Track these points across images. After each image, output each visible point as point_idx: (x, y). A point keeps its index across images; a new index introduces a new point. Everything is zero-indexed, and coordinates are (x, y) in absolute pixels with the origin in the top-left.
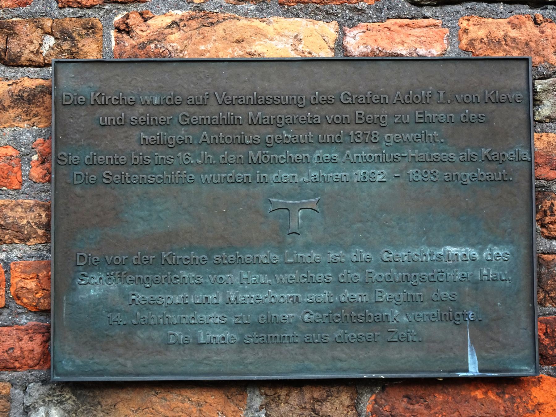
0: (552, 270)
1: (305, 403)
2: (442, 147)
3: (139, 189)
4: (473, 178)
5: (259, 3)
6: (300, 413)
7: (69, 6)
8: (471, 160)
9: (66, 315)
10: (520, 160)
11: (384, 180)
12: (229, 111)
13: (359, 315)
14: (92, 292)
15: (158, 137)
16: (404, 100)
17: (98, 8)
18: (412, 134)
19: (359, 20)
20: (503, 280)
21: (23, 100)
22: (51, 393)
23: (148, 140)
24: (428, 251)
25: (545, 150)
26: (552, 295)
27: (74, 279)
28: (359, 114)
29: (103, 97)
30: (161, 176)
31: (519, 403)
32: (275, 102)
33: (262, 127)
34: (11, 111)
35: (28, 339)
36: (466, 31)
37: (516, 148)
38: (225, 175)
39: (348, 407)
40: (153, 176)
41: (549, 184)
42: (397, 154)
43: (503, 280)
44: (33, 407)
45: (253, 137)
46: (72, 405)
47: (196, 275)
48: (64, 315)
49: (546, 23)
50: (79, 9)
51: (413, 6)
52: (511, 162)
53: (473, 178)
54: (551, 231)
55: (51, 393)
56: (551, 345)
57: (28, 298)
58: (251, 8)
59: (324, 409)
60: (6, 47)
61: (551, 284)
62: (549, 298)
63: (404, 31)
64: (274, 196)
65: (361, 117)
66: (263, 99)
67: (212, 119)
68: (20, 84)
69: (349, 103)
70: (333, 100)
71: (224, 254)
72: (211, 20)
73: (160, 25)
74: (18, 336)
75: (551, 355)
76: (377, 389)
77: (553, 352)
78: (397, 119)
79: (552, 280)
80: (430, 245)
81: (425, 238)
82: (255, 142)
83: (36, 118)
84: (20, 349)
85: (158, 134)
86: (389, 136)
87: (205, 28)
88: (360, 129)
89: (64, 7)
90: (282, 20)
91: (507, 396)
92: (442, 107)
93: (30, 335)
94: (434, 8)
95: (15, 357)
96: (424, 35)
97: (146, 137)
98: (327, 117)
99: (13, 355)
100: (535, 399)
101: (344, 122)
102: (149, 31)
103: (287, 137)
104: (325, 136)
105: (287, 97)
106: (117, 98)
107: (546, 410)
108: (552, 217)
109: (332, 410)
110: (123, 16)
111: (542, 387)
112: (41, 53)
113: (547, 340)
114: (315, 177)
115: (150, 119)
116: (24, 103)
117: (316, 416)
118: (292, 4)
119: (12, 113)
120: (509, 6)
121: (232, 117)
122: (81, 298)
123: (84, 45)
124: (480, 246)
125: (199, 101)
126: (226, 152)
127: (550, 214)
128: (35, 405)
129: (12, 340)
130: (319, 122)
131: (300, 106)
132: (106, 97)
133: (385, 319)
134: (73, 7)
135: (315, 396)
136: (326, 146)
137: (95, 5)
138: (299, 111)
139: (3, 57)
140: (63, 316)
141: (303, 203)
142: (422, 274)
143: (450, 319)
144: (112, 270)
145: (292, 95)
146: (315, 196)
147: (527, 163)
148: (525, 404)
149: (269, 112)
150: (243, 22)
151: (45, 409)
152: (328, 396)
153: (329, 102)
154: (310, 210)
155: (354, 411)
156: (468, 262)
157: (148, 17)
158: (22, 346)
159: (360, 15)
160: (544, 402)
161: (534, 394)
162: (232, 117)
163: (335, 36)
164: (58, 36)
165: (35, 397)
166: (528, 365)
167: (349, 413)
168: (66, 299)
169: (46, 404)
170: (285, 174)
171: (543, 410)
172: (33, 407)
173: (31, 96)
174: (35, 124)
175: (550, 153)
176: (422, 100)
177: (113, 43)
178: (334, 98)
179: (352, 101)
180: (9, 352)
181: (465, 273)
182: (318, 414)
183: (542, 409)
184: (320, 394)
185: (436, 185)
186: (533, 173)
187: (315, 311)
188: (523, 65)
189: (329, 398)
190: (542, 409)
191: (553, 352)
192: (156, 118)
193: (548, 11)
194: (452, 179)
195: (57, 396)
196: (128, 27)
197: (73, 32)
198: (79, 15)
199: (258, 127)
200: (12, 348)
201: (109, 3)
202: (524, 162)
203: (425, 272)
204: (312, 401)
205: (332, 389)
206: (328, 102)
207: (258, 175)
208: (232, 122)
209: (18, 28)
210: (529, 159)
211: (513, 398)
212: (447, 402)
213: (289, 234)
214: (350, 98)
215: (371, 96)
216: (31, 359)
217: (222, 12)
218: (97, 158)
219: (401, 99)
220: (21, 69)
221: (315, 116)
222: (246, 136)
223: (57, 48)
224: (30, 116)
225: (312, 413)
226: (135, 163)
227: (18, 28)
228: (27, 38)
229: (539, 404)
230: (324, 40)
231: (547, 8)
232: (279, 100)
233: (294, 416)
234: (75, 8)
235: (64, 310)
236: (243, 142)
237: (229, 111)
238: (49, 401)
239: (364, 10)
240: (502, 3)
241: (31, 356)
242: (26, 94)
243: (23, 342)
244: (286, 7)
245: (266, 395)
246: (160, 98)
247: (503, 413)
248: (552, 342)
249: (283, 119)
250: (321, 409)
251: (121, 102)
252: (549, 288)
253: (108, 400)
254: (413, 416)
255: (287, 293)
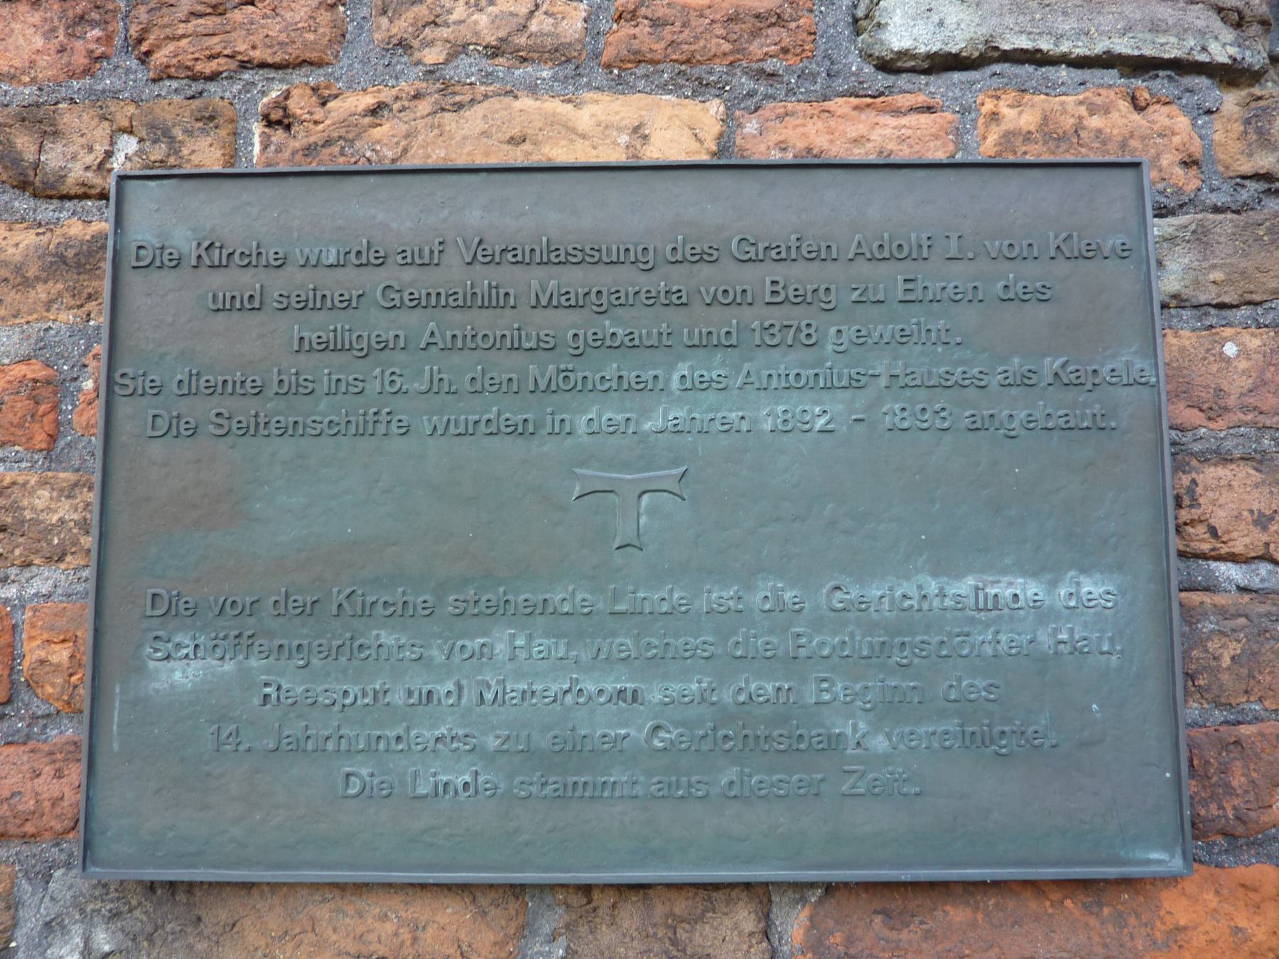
0: (1199, 626)
1: (655, 925)
2: (958, 354)
3: (286, 448)
4: (1029, 422)
5: (559, 65)
6: (643, 948)
7: (170, 77)
8: (1026, 381)
9: (119, 726)
10: (1131, 381)
11: (830, 427)
12: (485, 278)
13: (776, 733)
14: (178, 675)
15: (331, 335)
16: (872, 253)
17: (226, 78)
18: (891, 326)
19: (767, 97)
20: (1102, 653)
21: (65, 263)
22: (97, 893)
23: (310, 342)
24: (932, 587)
25: (1174, 365)
26: (1201, 682)
27: (140, 646)
28: (772, 282)
29: (217, 251)
30: (336, 419)
31: (1135, 927)
32: (589, 256)
33: (561, 312)
34: (40, 287)
35: (53, 773)
36: (994, 117)
37: (1123, 355)
38: (476, 417)
39: (751, 934)
40: (318, 419)
41: (1184, 439)
42: (858, 370)
43: (1102, 653)
44: (58, 924)
45: (538, 334)
46: (141, 921)
47: (409, 639)
48: (115, 728)
49: (1157, 107)
50: (190, 82)
51: (880, 72)
52: (1111, 388)
53: (1029, 422)
54: (1191, 540)
55: (97, 893)
56: (1203, 795)
57: (53, 685)
58: (545, 74)
59: (698, 939)
60: (39, 159)
61: (1198, 659)
62: (1193, 689)
63: (863, 117)
64: (583, 464)
65: (778, 288)
66: (562, 252)
67: (448, 296)
68: (58, 231)
69: (750, 259)
70: (715, 253)
71: (472, 592)
72: (458, 98)
73: (353, 109)
74: (32, 768)
75: (1203, 817)
76: (813, 894)
77: (1207, 811)
78: (858, 292)
79: (1201, 649)
80: (935, 574)
81: (924, 557)
82: (542, 345)
83: (94, 303)
84: (33, 794)
85: (332, 328)
86: (839, 331)
87: (447, 115)
88: (777, 316)
89: (160, 79)
90: (605, 97)
91: (1106, 911)
92: (957, 267)
93: (57, 766)
94: (923, 77)
95: (24, 812)
96: (908, 124)
97: (306, 334)
98: (702, 289)
99: (20, 808)
100: (1168, 918)
101: (741, 300)
102: (328, 122)
103: (613, 334)
104: (697, 331)
105: (614, 248)
106: (247, 253)
107: (1195, 943)
108: (1193, 510)
109: (716, 942)
110: (279, 93)
111: (1183, 888)
112: (110, 170)
113: (1194, 783)
114: (676, 422)
115: (315, 295)
116: (67, 271)
117: (679, 954)
118: (630, 65)
119: (41, 292)
120: (1079, 72)
121: (494, 291)
122: (154, 690)
123: (193, 151)
124: (1049, 576)
125: (421, 257)
126: (479, 367)
127: (1189, 503)
128: (63, 920)
129: (20, 775)
130: (684, 300)
131: (641, 266)
132: (318, 292)
133: (834, 743)
134: (177, 78)
135: (677, 911)
136: (701, 353)
137: (221, 73)
138: (643, 278)
139: (32, 179)
140: (112, 729)
141: (650, 479)
142: (919, 638)
143: (983, 743)
144: (223, 628)
145: (624, 244)
146: (675, 463)
147: (1145, 391)
148: (1148, 929)
149: (574, 279)
150: (525, 102)
151: (85, 930)
152: (704, 912)
153: (706, 257)
154: (665, 494)
155: (764, 944)
156: (1021, 612)
157: (329, 96)
158: (39, 789)
159: (771, 86)
160: (1190, 924)
161: (1166, 905)
162: (494, 291)
163: (717, 128)
164: (144, 134)
165: (62, 903)
166: (1165, 847)
167: (752, 950)
168: (121, 692)
169: (86, 917)
170: (610, 415)
171: (1188, 942)
172: (58, 924)
173: (81, 256)
174: (92, 316)
175: (1185, 372)
176: (910, 254)
177: (257, 149)
178: (717, 250)
179: (757, 255)
180: (12, 802)
181: (1016, 637)
182: (684, 951)
183: (1185, 941)
184: (686, 907)
185: (948, 437)
186: (1164, 412)
187: (677, 724)
188: (1129, 174)
189: (710, 915)
190: (1185, 941)
191: (1207, 811)
192: (328, 294)
193: (1158, 81)
194: (983, 425)
195: (112, 901)
196: (286, 115)
197: (174, 126)
198: (190, 93)
199: (550, 312)
200: (19, 793)
201: (252, 69)
202: (1141, 387)
203: (926, 633)
204: (670, 921)
205: (715, 894)
206: (701, 258)
207: (549, 418)
208: (498, 301)
209: (65, 120)
210: (1153, 380)
211: (1120, 914)
212: (974, 925)
213: (618, 548)
214: (752, 249)
215: (798, 244)
216: (58, 817)
217: (482, 83)
218: (198, 380)
219: (864, 250)
220: (68, 204)
221: (675, 289)
222: (523, 333)
223: (140, 157)
224: (80, 298)
225: (671, 948)
226: (281, 391)
227: (65, 120)
228: (83, 140)
229: (1177, 929)
230: (696, 135)
231: (1157, 76)
232: (597, 254)
233: (631, 954)
234: (182, 78)
235: (116, 715)
236: (516, 345)
237: (485, 278)
238: (93, 911)
239: (780, 75)
240: (1063, 66)
241: (58, 811)
242: (70, 253)
243: (41, 780)
244: (616, 71)
245: (568, 906)
246: (338, 251)
247: (1100, 950)
248: (1204, 787)
249: (605, 293)
250: (691, 941)
251: (251, 260)
252: (1193, 667)
253: (217, 914)
254: (897, 956)
255: (614, 682)
